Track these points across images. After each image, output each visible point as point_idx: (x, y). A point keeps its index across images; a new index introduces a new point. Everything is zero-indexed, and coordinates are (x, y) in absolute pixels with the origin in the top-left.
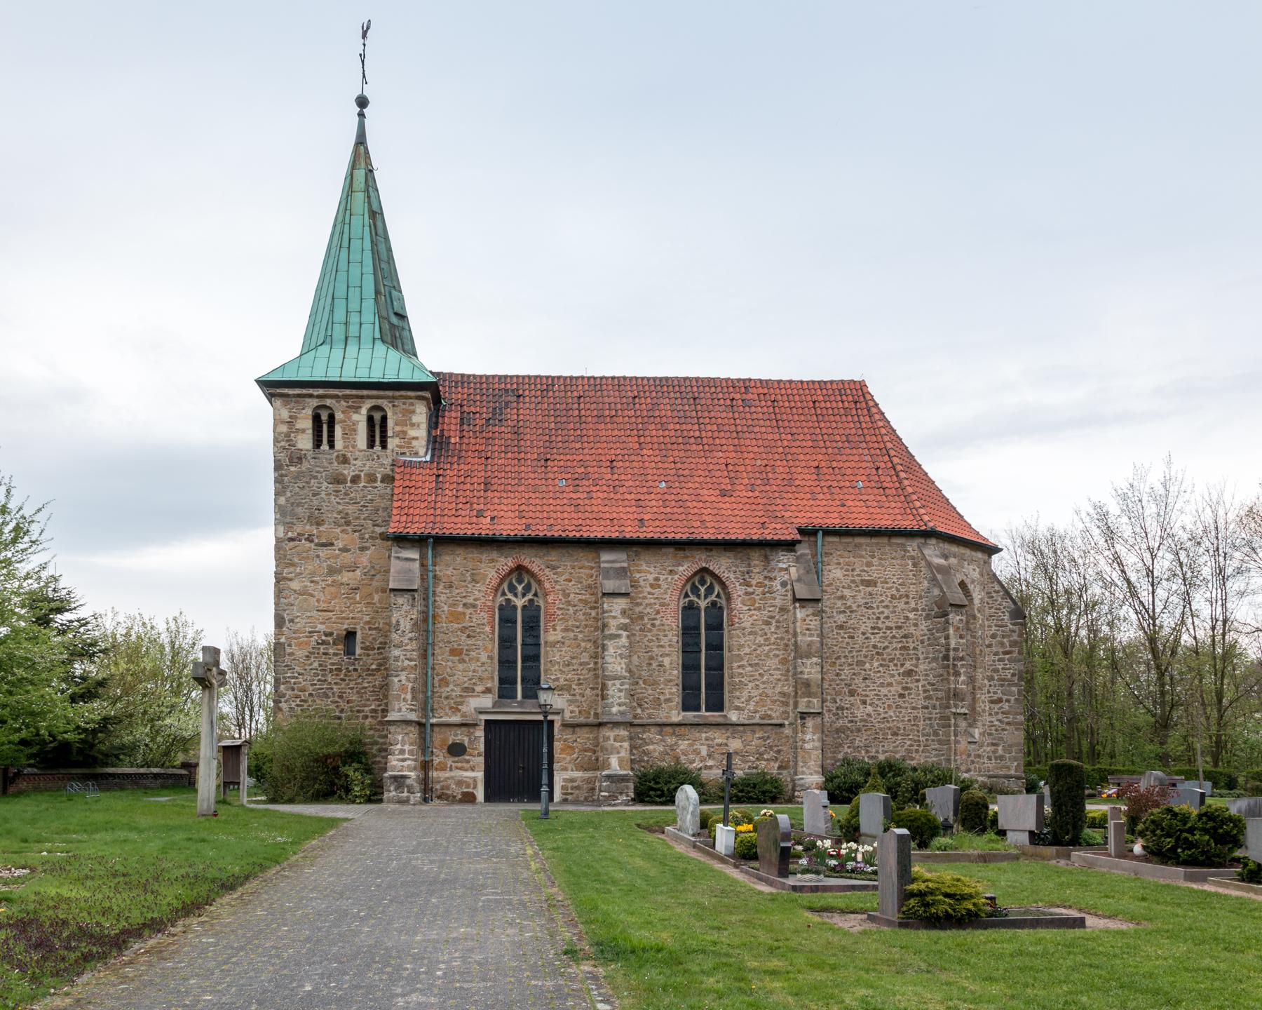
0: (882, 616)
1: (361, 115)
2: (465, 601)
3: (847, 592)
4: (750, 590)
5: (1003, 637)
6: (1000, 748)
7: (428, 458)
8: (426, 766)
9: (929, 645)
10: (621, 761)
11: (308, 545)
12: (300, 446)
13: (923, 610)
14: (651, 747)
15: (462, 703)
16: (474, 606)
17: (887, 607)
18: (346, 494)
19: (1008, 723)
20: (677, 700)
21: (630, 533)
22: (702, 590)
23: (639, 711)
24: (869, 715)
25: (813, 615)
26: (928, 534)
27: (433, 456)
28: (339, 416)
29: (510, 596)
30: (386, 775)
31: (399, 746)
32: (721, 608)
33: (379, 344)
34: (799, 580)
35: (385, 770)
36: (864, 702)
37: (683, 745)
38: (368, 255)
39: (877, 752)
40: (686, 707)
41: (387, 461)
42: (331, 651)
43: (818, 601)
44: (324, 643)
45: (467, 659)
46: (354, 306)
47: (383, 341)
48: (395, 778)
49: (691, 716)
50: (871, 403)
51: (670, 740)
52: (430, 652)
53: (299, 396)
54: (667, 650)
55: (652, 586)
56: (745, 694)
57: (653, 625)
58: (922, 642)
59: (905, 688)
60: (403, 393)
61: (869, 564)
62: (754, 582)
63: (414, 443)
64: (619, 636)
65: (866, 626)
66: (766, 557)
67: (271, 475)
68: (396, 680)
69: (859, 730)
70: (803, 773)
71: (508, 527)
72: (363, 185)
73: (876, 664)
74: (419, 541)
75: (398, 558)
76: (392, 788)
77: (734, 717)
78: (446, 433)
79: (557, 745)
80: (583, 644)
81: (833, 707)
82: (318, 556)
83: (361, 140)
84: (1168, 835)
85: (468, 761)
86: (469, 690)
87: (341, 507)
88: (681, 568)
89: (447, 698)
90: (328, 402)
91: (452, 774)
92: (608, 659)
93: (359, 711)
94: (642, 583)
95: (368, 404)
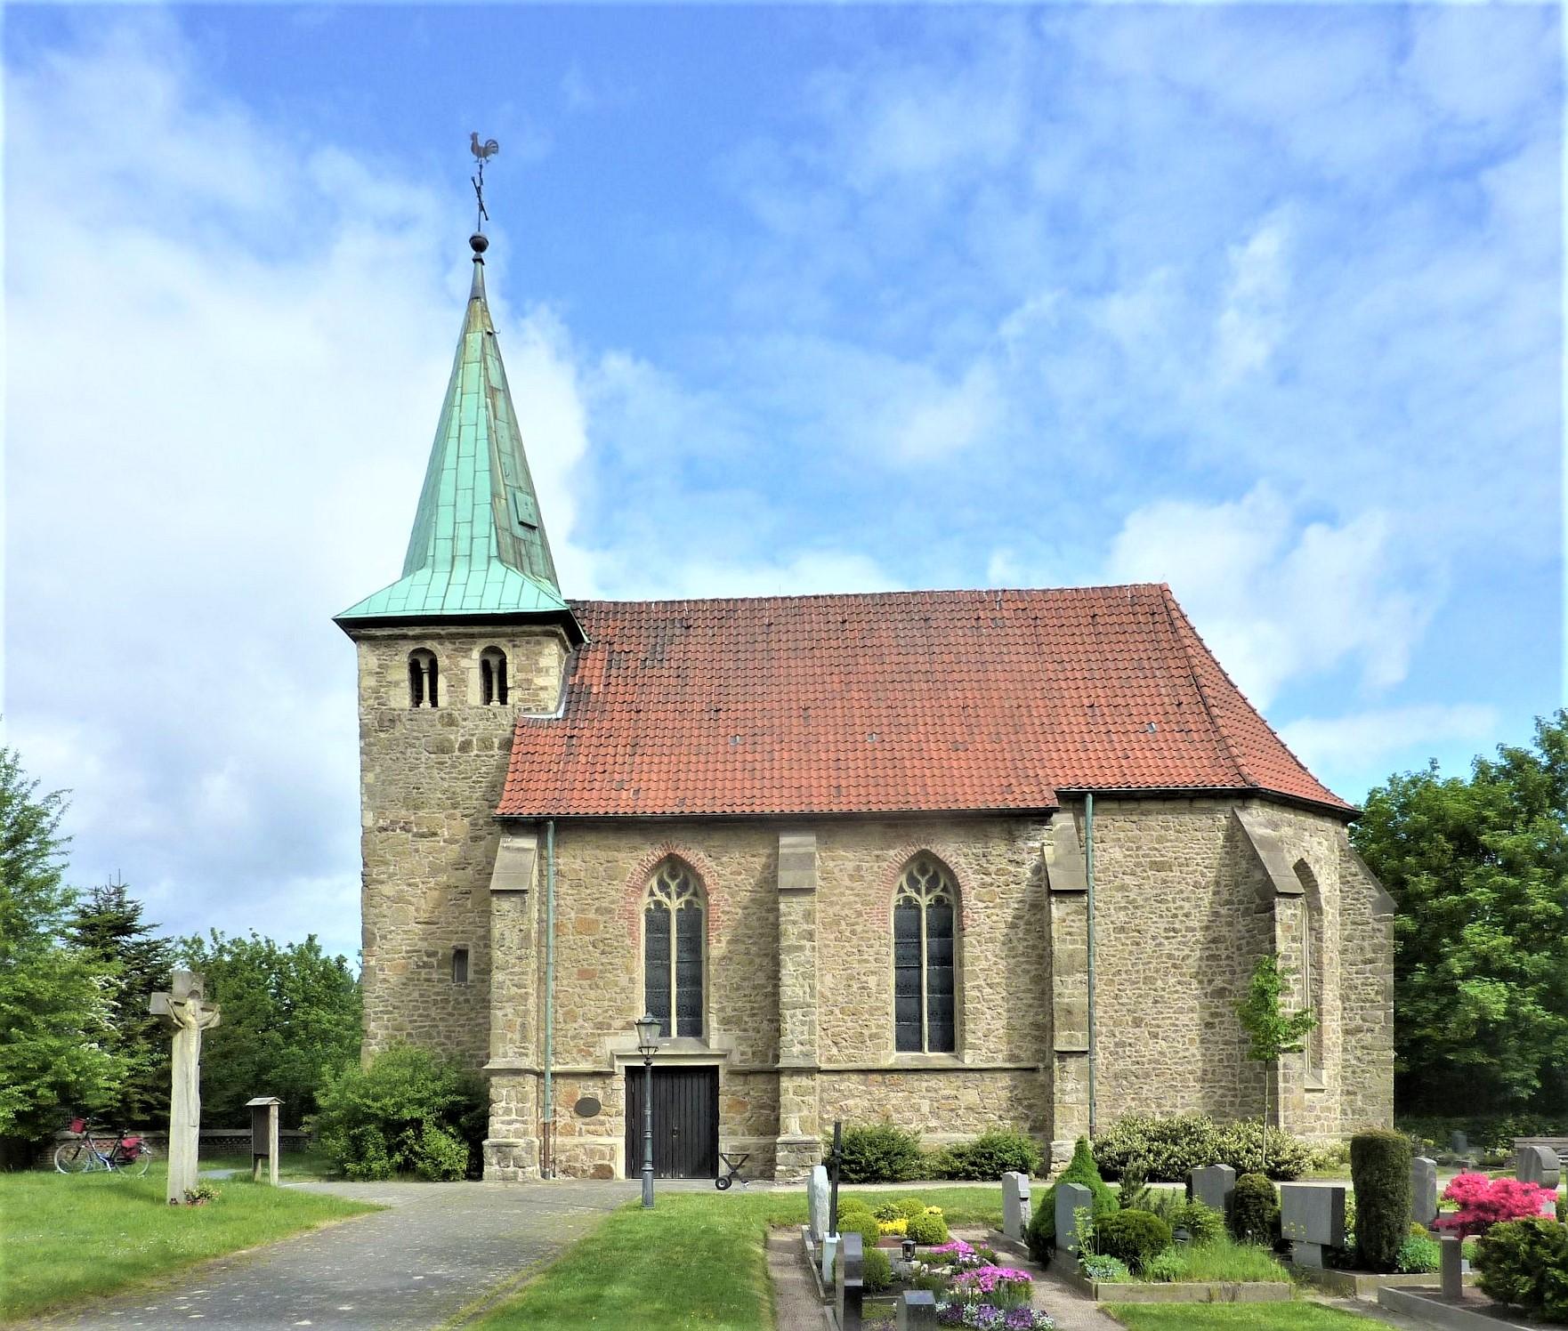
1: (478, 260)
4: (988, 879)
6: (1359, 1097)
7: (560, 714)
8: (546, 1129)
9: (1249, 953)
10: (803, 1122)
11: (404, 835)
12: (393, 704)
13: (1241, 902)
14: (851, 1102)
16: (610, 911)
17: (1188, 899)
20: (891, 1035)
21: (820, 805)
22: (923, 881)
23: (835, 1051)
25: (1076, 912)
26: (1248, 795)
27: (567, 710)
28: (443, 662)
29: (661, 896)
30: (485, 1143)
31: (503, 1104)
32: (949, 907)
33: (495, 564)
34: (1055, 864)
35: (486, 1137)
36: (1156, 1036)
37: (896, 1098)
38: (483, 445)
40: (901, 1046)
41: (506, 722)
42: (435, 976)
43: (1081, 893)
44: (425, 965)
46: (464, 514)
47: (502, 561)
48: (498, 1147)
49: (908, 1058)
50: (1175, 614)
51: (879, 1092)
52: (551, 974)
54: (873, 966)
55: (851, 877)
56: (983, 1026)
57: (853, 932)
58: (1239, 949)
59: (1213, 1015)
60: (526, 628)
61: (1160, 840)
62: (993, 868)
63: (542, 695)
64: (801, 948)
65: (1157, 927)
66: (1010, 833)
67: (355, 744)
68: (500, 1013)
69: (1147, 1075)
71: (656, 801)
72: (478, 353)
73: (1172, 981)
74: (534, 826)
75: (508, 848)
76: (494, 1161)
77: (969, 1060)
78: (587, 681)
79: (723, 1100)
80: (758, 960)
81: (1110, 1043)
82: (417, 851)
84: (1525, 1270)
85: (602, 1123)
86: (603, 1027)
88: (892, 853)
89: (573, 1038)
90: (428, 645)
91: (582, 1140)
93: (471, 1056)
94: (837, 874)
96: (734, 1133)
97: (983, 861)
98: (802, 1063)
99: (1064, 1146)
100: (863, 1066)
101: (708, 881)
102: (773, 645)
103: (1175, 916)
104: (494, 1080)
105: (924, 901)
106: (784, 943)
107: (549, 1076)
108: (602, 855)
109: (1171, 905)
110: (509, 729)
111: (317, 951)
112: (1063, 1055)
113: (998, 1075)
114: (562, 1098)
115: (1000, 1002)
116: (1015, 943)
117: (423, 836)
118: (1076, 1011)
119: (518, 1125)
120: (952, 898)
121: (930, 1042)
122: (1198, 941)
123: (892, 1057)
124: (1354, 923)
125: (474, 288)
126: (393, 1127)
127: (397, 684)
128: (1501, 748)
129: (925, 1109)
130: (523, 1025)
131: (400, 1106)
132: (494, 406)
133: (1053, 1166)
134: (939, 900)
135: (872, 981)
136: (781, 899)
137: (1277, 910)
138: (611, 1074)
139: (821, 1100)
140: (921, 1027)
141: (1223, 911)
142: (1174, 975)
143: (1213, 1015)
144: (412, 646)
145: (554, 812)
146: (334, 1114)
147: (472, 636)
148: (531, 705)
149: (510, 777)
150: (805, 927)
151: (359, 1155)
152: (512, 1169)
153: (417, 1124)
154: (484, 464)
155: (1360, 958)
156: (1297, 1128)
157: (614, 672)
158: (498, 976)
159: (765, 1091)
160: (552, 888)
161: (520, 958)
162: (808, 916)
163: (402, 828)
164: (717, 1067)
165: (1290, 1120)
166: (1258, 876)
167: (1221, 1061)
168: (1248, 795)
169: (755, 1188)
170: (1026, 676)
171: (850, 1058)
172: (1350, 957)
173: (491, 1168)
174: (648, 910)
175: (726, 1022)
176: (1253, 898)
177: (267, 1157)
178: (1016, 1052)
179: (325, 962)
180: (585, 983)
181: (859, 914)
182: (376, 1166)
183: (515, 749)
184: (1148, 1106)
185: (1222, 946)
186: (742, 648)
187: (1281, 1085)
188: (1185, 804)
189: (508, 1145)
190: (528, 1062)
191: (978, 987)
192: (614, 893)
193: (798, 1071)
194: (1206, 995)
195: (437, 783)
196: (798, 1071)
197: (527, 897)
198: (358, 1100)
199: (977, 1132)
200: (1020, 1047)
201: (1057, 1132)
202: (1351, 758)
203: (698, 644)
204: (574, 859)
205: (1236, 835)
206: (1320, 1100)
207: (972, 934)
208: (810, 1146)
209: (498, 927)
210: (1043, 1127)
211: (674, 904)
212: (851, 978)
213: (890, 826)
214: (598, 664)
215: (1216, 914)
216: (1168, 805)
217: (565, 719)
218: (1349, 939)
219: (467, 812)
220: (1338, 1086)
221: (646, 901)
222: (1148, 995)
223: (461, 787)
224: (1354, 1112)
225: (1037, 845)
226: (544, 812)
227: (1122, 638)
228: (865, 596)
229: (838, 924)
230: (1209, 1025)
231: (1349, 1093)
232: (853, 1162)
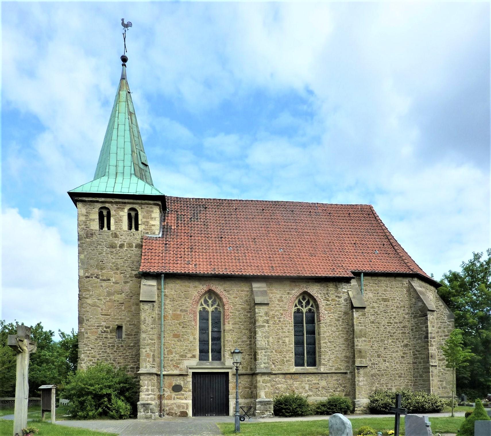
0: (392, 317)
2: (181, 308)
4: (328, 303)
5: (444, 328)
6: (444, 383)
7: (160, 235)
8: (160, 397)
9: (416, 331)
11: (97, 280)
12: (92, 228)
13: (412, 314)
14: (280, 386)
16: (186, 311)
18: (116, 254)
21: (267, 272)
24: (387, 367)
25: (362, 315)
27: (163, 234)
28: (113, 212)
29: (205, 306)
30: (138, 403)
31: (146, 387)
34: (354, 297)
35: (139, 401)
36: (385, 361)
37: (296, 384)
38: (127, 132)
39: (392, 386)
40: (297, 365)
41: (139, 237)
42: (109, 336)
44: (105, 332)
46: (121, 157)
47: (136, 176)
48: (144, 405)
49: (299, 369)
51: (290, 382)
52: (163, 336)
53: (91, 201)
54: (287, 334)
55: (279, 300)
57: (280, 321)
58: (412, 330)
59: (404, 353)
60: (146, 201)
61: (385, 291)
62: (330, 299)
63: (153, 228)
64: (264, 326)
65: (384, 322)
66: (336, 286)
68: (144, 350)
69: (382, 375)
70: (359, 398)
71: (203, 269)
72: (125, 99)
73: (390, 341)
74: (156, 276)
75: (145, 285)
76: (142, 410)
77: (322, 369)
78: (169, 224)
80: (244, 331)
82: (102, 286)
83: (123, 78)
85: (183, 395)
86: (183, 356)
87: (114, 261)
88: (293, 292)
89: (171, 360)
90: (107, 205)
91: (175, 401)
94: (273, 299)
95: (128, 207)
97: (327, 296)
98: (265, 371)
99: (363, 400)
100: (284, 372)
102: (238, 216)
103: (391, 318)
106: (257, 324)
107: (162, 376)
108: (183, 289)
110: (139, 240)
111: (42, 328)
112: (359, 368)
114: (167, 385)
115: (333, 348)
117: (104, 280)
119: (152, 396)
120: (315, 309)
123: (294, 369)
125: (122, 75)
126: (98, 397)
127: (94, 220)
128: (450, 271)
129: (307, 388)
130: (154, 355)
131: (101, 389)
132: (131, 119)
133: (356, 409)
135: (287, 340)
136: (256, 307)
137: (428, 316)
138: (187, 375)
140: (304, 358)
141: (406, 317)
142: (391, 339)
143: (404, 353)
144: (100, 205)
145: (164, 271)
146: (72, 392)
147: (125, 203)
149: (143, 257)
150: (265, 318)
151: (83, 409)
152: (149, 414)
153: (109, 396)
154: (128, 139)
155: (443, 334)
158: (143, 335)
159: (247, 382)
160: (163, 302)
161: (152, 328)
162: (266, 314)
163: (96, 277)
164: (228, 373)
166: (420, 304)
167: (407, 370)
169: (252, 420)
170: (330, 232)
173: (141, 413)
176: (422, 313)
177: (50, 411)
178: (339, 366)
179: (46, 333)
180: (176, 339)
181: (282, 314)
182: (91, 413)
183: (144, 247)
184: (383, 386)
186: (227, 216)
187: (431, 378)
188: (393, 279)
189: (148, 404)
190: (154, 371)
191: (325, 343)
192: (188, 304)
193: (264, 374)
195: (110, 259)
196: (264, 374)
197: (155, 304)
198: (83, 386)
199: (326, 396)
200: (341, 365)
201: (357, 396)
202: (439, 266)
203: (211, 215)
204: (173, 288)
205: (411, 289)
207: (324, 323)
208: (268, 403)
209: (143, 316)
210: (352, 393)
212: (279, 338)
213: (293, 282)
214: (173, 219)
217: (163, 238)
219: (122, 271)
221: (199, 308)
223: (120, 261)
224: (442, 388)
226: (160, 271)
227: (360, 222)
228: (269, 202)
229: (274, 318)
232: (287, 409)
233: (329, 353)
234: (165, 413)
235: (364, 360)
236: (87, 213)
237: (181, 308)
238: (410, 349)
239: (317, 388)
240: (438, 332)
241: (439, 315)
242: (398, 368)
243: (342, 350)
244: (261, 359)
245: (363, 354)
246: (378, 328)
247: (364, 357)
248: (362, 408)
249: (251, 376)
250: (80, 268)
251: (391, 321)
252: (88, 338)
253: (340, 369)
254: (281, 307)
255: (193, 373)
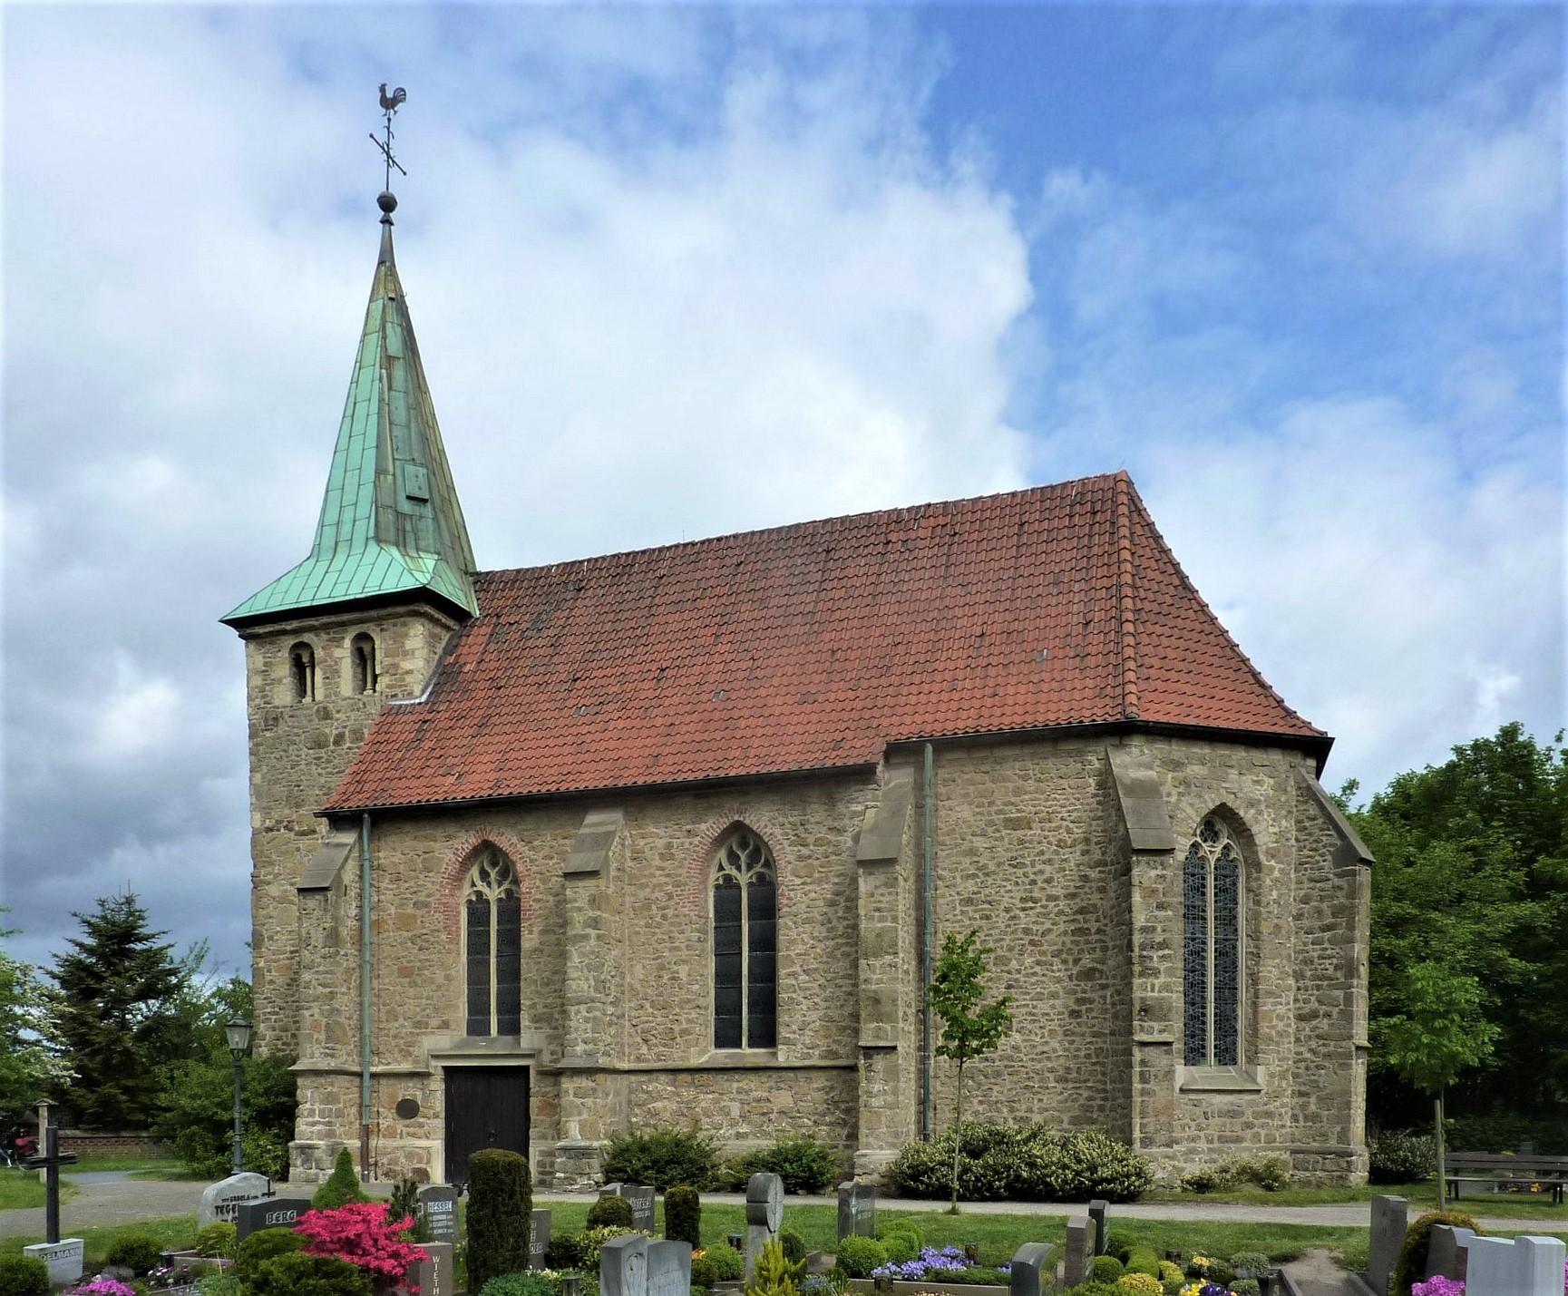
0: (1040, 878)
1: (387, 222)
2: (415, 898)
3: (979, 843)
4: (805, 851)
5: (1322, 899)
6: (1313, 1100)
8: (366, 1133)
12: (277, 702)
14: (659, 1105)
15: (411, 1045)
16: (426, 905)
18: (329, 761)
19: (1328, 1056)
22: (743, 857)
23: (644, 1050)
24: (1015, 1048)
25: (886, 885)
28: (319, 654)
29: (481, 886)
31: (308, 1106)
33: (372, 544)
37: (706, 1100)
39: (1030, 1110)
40: (720, 1043)
45: (419, 980)
48: (302, 1148)
49: (724, 1056)
51: (688, 1093)
53: (271, 634)
54: (684, 954)
57: (664, 917)
59: (1079, 1001)
60: (390, 610)
61: (1018, 792)
62: (811, 839)
63: (409, 679)
64: (585, 937)
65: (1011, 896)
68: (307, 1013)
69: (998, 1074)
70: (868, 1146)
73: (1029, 961)
76: (299, 1162)
77: (783, 1056)
78: (461, 661)
82: (298, 849)
85: (421, 1126)
86: (421, 1025)
87: (322, 780)
88: (703, 826)
89: (395, 1037)
91: (402, 1143)
92: (572, 973)
94: (648, 854)
95: (352, 632)
96: (544, 1137)
100: (671, 1064)
101: (520, 867)
103: (1034, 882)
104: (300, 1081)
105: (743, 878)
106: (570, 933)
107: (366, 1076)
108: (422, 846)
109: (1029, 869)
112: (870, 1051)
113: (813, 1074)
115: (817, 990)
116: (835, 922)
117: (303, 834)
118: (884, 999)
121: (750, 1037)
122: (1061, 913)
124: (1311, 880)
129: (735, 1112)
134: (761, 877)
137: (1135, 872)
139: (629, 1102)
141: (1093, 874)
142: (1030, 955)
143: (1079, 1001)
144: (291, 641)
145: (370, 804)
147: (343, 624)
148: (397, 691)
150: (591, 913)
154: (372, 441)
156: (1160, 1138)
157: (492, 647)
164: (527, 1068)
165: (1151, 1128)
167: (1088, 1056)
168: (1123, 730)
171: (659, 1057)
172: (1306, 923)
174: (470, 902)
175: (536, 1019)
178: (834, 1047)
184: (998, 1111)
185: (1092, 917)
187: (1137, 1086)
188: (1048, 748)
189: (311, 1147)
191: (793, 975)
194: (1070, 977)
200: (838, 1042)
201: (862, 1139)
203: (584, 610)
204: (397, 850)
206: (1251, 1104)
208: (584, 1153)
211: (493, 894)
215: (1085, 878)
216: (1027, 750)
218: (1305, 900)
220: (1288, 1086)
221: (466, 892)
222: (999, 979)
224: (1306, 1117)
225: (860, 808)
229: (649, 909)
230: (1074, 1014)
231: (1301, 1094)
233: (805, 1005)
234: (380, 1172)
235: (888, 1027)
236: (265, 664)
237: (415, 898)
238: (1104, 987)
239: (764, 1114)
240: (1298, 917)
241: (1306, 852)
242: (1055, 1050)
243: (843, 997)
244: (576, 1030)
245: (886, 1008)
246: (988, 918)
247: (891, 1018)
248: (875, 1176)
249: (552, 1079)
250: (254, 808)
251: (1036, 895)
252: (271, 982)
253: (835, 1055)
254: (668, 875)
255: (445, 1068)
